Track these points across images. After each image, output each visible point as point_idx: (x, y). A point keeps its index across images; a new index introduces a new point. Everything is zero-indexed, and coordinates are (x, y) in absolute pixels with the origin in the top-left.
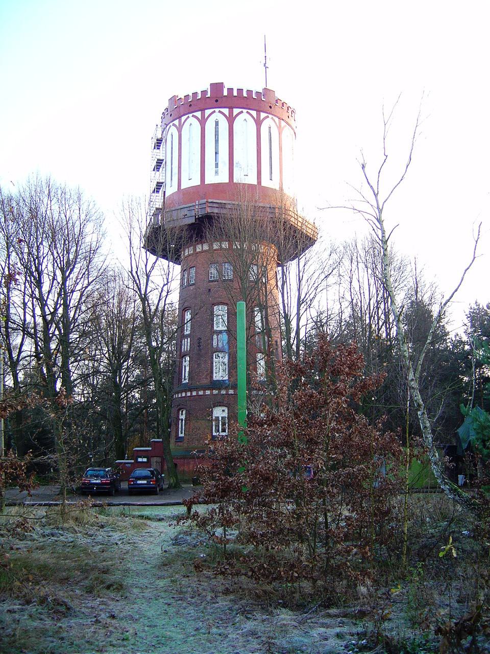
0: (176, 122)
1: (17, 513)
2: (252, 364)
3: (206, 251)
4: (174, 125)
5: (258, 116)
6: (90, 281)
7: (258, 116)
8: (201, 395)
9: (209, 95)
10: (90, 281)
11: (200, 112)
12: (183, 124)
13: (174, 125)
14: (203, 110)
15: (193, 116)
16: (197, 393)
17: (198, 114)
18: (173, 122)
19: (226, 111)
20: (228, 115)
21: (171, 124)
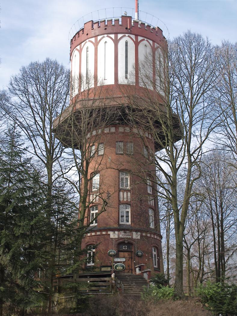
0: (78, 47)
1: (108, 296)
2: (171, 179)
3: (112, 133)
4: (77, 50)
5: (137, 39)
6: (203, 109)
7: (137, 39)
8: (104, 235)
9: (120, 23)
10: (203, 109)
11: (94, 38)
12: (83, 47)
13: (77, 50)
14: (116, 34)
15: (89, 41)
16: (106, 233)
17: (93, 40)
18: (76, 48)
19: (113, 36)
20: (94, 42)
21: (75, 49)
